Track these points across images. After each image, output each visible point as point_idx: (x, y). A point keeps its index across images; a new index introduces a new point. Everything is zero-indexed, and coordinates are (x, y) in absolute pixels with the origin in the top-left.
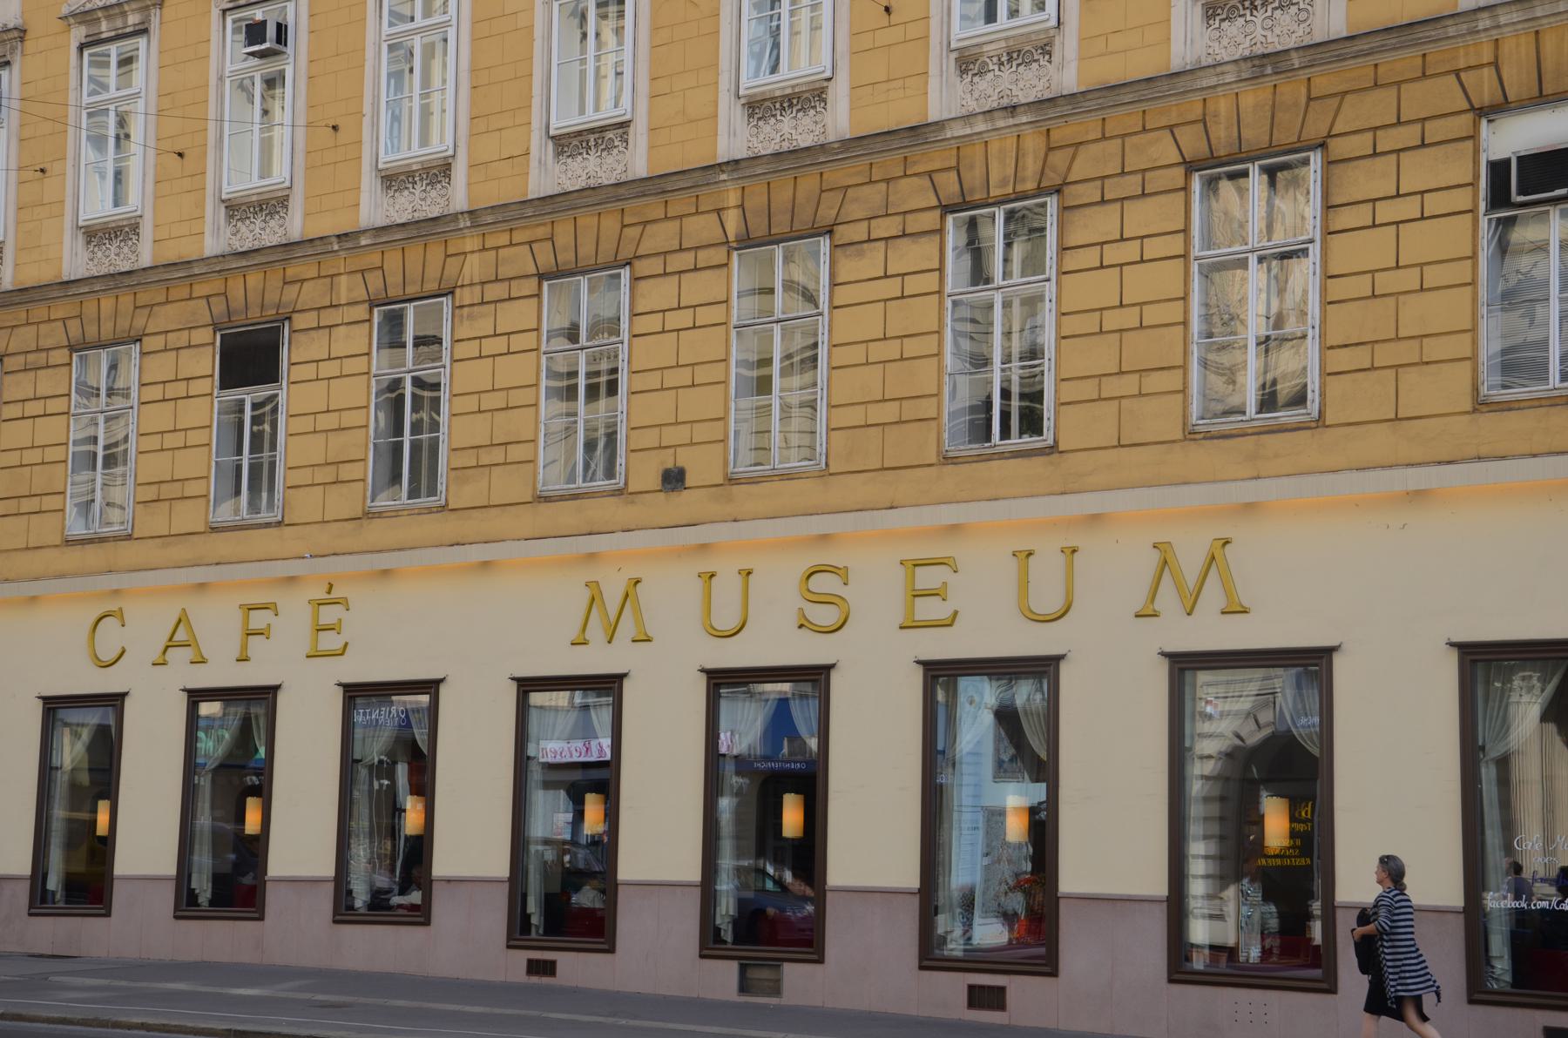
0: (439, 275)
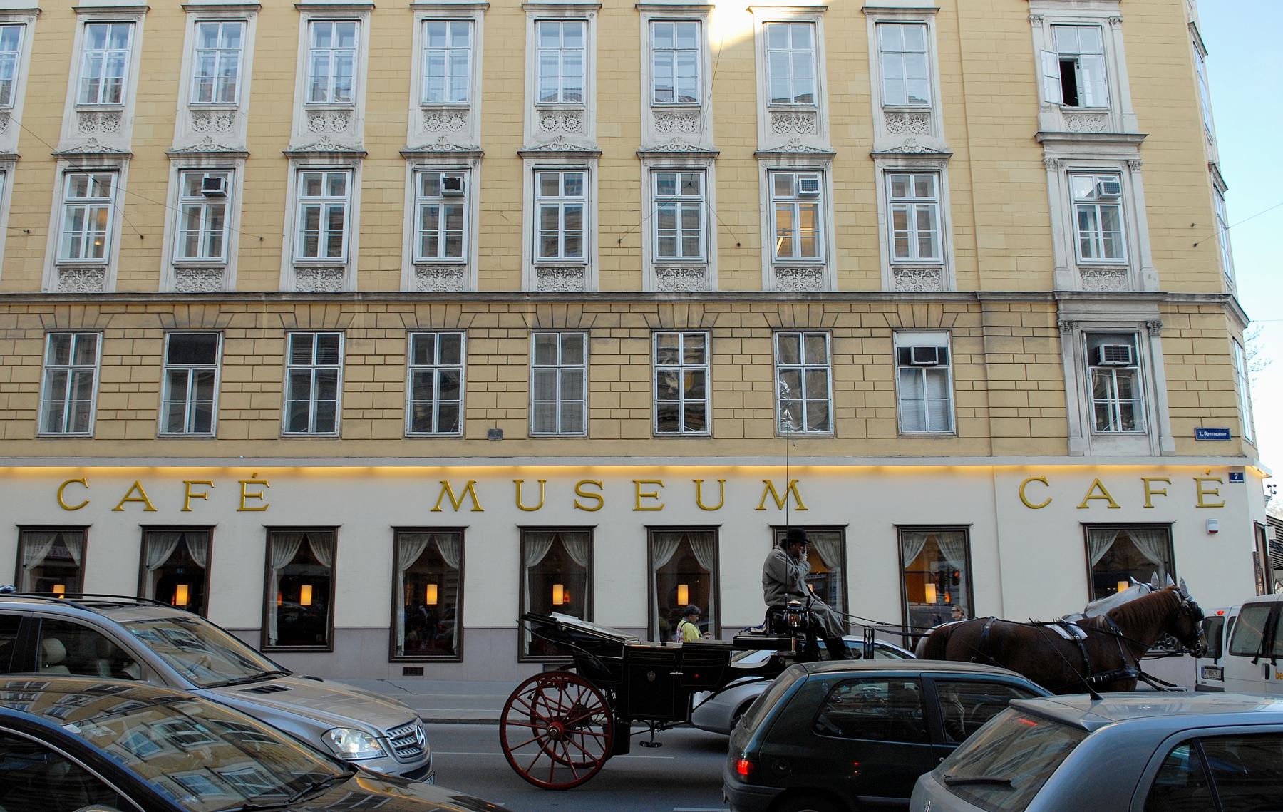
0: (336, 321)
